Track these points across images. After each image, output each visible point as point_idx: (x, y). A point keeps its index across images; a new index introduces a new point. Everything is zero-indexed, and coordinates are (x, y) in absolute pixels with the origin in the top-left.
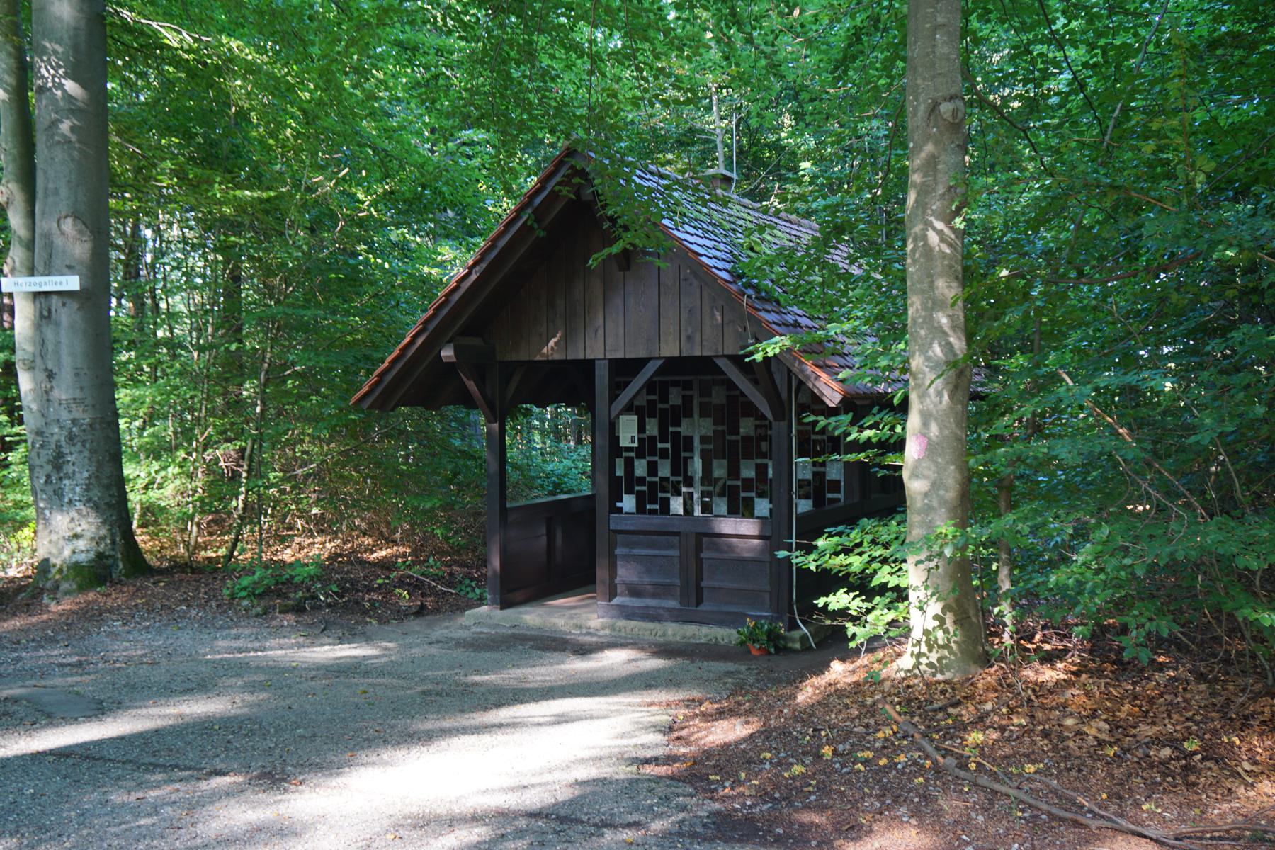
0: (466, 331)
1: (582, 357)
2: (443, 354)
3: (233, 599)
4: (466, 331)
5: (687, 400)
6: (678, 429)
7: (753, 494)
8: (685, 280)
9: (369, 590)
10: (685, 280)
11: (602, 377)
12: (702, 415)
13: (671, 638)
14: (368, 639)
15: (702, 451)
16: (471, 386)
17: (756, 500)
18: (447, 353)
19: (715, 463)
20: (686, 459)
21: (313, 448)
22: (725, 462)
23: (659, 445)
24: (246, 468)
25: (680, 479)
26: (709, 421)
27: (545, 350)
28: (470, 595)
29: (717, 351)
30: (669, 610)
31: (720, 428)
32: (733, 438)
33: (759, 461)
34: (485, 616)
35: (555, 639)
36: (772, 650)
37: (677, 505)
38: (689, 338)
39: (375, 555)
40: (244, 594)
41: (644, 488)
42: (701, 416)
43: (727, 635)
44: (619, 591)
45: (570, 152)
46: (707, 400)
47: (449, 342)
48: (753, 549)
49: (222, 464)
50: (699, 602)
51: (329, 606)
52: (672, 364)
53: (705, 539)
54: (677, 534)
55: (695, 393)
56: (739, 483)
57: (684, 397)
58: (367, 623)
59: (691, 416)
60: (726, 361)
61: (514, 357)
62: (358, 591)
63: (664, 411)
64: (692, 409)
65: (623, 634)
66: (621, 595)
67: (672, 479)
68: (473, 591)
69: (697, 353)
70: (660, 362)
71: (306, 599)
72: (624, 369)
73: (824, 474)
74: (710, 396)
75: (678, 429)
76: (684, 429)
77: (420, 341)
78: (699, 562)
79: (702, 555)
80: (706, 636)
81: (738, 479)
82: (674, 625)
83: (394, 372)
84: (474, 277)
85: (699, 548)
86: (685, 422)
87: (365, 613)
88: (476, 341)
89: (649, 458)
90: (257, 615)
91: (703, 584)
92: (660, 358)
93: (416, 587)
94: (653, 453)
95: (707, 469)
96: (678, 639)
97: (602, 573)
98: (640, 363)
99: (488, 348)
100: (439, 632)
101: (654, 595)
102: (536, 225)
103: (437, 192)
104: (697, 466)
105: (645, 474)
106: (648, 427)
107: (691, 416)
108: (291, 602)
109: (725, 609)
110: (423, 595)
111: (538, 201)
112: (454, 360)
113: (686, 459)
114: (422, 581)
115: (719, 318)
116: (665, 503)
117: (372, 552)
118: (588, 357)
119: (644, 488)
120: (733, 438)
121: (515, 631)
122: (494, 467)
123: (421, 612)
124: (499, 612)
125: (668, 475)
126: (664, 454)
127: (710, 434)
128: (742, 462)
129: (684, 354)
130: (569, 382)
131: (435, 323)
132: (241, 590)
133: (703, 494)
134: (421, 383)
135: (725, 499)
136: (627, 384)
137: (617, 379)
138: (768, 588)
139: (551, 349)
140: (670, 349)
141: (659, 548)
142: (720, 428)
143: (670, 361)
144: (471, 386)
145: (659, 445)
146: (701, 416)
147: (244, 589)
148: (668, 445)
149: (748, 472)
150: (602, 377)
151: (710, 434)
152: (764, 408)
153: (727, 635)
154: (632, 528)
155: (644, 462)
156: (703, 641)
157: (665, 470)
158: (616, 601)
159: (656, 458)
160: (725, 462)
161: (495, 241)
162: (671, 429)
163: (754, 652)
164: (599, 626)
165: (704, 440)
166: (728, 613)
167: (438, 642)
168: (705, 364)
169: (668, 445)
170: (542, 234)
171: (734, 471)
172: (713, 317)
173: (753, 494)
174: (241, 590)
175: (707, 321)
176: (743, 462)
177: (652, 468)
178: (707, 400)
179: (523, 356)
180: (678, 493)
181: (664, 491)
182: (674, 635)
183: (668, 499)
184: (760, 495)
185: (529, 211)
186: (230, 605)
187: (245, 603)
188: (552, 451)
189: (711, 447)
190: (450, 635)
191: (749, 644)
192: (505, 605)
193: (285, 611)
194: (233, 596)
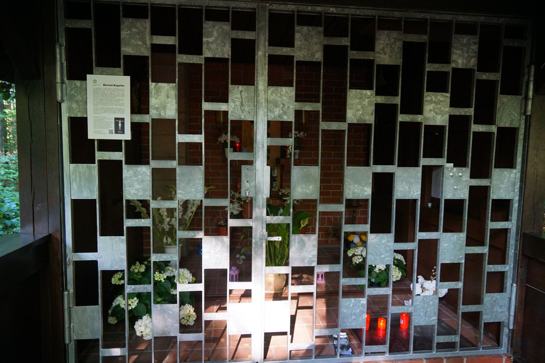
6: (222, 107)
12: (275, 81)
15: (269, 149)
19: (296, 172)
22: (315, 171)
23: (181, 138)
31: (308, 107)
32: (334, 126)
33: (380, 169)
46: (285, 51)
57: (235, 44)
59: (248, 80)
73: (485, 190)
74: (291, 44)
75: (222, 107)
76: (236, 105)
81: (338, 201)
86: (236, 93)
89: (154, 164)
104: (259, 178)
107: (248, 80)
113: (237, 167)
120: (334, 126)
126: (190, 155)
127: (290, 117)
133: (272, 229)
142: (308, 107)
145: (181, 138)
151: (290, 117)
157: (191, 185)
159: (173, 164)
160: (315, 171)
165: (277, 128)
169: (199, 138)
171: (331, 186)
173: (367, 227)
176: (350, 171)
178: (285, 51)
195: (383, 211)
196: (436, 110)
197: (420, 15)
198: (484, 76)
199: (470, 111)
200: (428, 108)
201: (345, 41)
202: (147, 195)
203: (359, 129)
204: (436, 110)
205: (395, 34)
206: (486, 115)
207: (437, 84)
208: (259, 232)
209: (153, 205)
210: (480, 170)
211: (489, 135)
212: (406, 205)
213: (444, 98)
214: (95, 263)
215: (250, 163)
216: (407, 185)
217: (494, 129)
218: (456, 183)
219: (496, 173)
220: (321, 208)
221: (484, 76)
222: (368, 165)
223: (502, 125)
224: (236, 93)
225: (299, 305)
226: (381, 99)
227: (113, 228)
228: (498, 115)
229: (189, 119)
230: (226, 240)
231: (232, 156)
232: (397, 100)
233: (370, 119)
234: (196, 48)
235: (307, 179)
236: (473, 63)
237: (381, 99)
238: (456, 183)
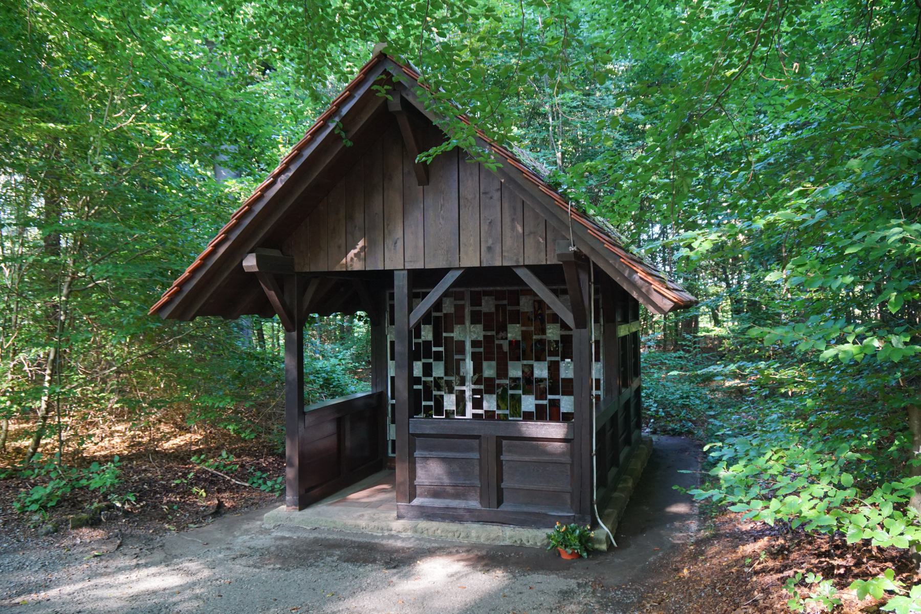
0: (267, 243)
1: (381, 268)
2: (244, 264)
3: (24, 512)
4: (267, 243)
5: (459, 309)
6: (452, 335)
8: (485, 193)
9: (167, 490)
10: (485, 193)
11: (401, 284)
12: (474, 321)
13: (474, 540)
14: (168, 560)
15: (473, 354)
16: (272, 295)
17: (523, 396)
18: (250, 262)
19: (485, 364)
20: (458, 361)
21: (118, 347)
22: (494, 363)
23: (434, 349)
24: (48, 372)
26: (479, 328)
27: (344, 260)
28: (263, 488)
29: (517, 261)
30: (470, 511)
31: (489, 333)
34: (283, 518)
35: (361, 546)
36: (585, 554)
37: (449, 402)
38: (489, 249)
39: (171, 442)
40: (35, 507)
41: (420, 387)
42: (472, 323)
43: (534, 537)
44: (418, 491)
45: (381, 58)
46: (478, 308)
47: (251, 252)
48: (559, 450)
49: (26, 368)
50: (500, 502)
51: (126, 513)
52: (472, 276)
53: (504, 442)
54: (478, 437)
55: (467, 303)
58: (166, 530)
60: (527, 271)
61: (313, 269)
62: (156, 492)
63: (437, 319)
64: (464, 317)
65: (425, 536)
66: (421, 496)
67: (445, 378)
68: (265, 483)
69: (498, 263)
70: (458, 273)
71: (102, 509)
72: (423, 279)
75: (452, 335)
76: (457, 334)
77: (222, 250)
78: (500, 464)
79: (502, 458)
80: (511, 538)
82: (476, 525)
83: (194, 282)
84: (279, 185)
85: (499, 452)
86: (457, 329)
87: (163, 518)
88: (276, 253)
89: (424, 361)
90: (47, 534)
91: (503, 485)
93: (212, 483)
94: (428, 356)
95: (478, 369)
96: (482, 540)
97: (401, 472)
99: (286, 258)
100: (241, 540)
101: (456, 496)
102: (343, 134)
103: (230, 121)
104: (469, 365)
105: (421, 375)
106: (423, 333)
108: (84, 515)
109: (526, 509)
110: (219, 491)
111: (345, 110)
112: (257, 270)
113: (458, 361)
114: (217, 476)
115: (520, 229)
116: (439, 402)
117: (168, 440)
119: (420, 387)
121: (315, 535)
122: (294, 373)
123: (219, 511)
124: (298, 513)
125: (442, 375)
126: (438, 357)
128: (510, 363)
129: (484, 265)
130: (367, 292)
131: (238, 232)
132: (33, 502)
133: (475, 392)
134: (222, 293)
136: (425, 295)
137: (414, 291)
138: (569, 488)
139: (353, 260)
140: (470, 260)
141: (459, 451)
142: (489, 333)
143: (469, 271)
144: (272, 295)
145: (434, 349)
146: (472, 323)
147: (36, 501)
148: (441, 349)
150: (401, 284)
152: (569, 319)
153: (534, 537)
154: (432, 432)
156: (508, 542)
157: (439, 370)
158: (416, 502)
159: (431, 361)
160: (494, 363)
161: (300, 150)
162: (444, 335)
163: (565, 557)
164: (401, 529)
165: (475, 344)
166: (534, 514)
167: (242, 556)
168: (505, 274)
169: (441, 349)
170: (349, 144)
171: (502, 371)
172: (513, 228)
173: (520, 392)
174: (33, 502)
175: (507, 232)
176: (510, 363)
177: (427, 370)
178: (478, 308)
179: (322, 266)
180: (451, 391)
181: (439, 389)
182: (478, 537)
183: (442, 396)
185: (337, 119)
186: (20, 520)
187: (35, 517)
188: (337, 353)
189: (482, 350)
190: (252, 544)
191: (561, 548)
192: (304, 503)
193: (78, 525)
194: (23, 509)
197: (477, 289)
200: (548, 331)
201: (505, 302)
202: (523, 396)
208: (468, 394)
209: (423, 379)
211: (419, 344)
215: (464, 360)
226: (524, 328)
229: (437, 341)
231: (456, 357)
235: (490, 367)
237: (524, 328)
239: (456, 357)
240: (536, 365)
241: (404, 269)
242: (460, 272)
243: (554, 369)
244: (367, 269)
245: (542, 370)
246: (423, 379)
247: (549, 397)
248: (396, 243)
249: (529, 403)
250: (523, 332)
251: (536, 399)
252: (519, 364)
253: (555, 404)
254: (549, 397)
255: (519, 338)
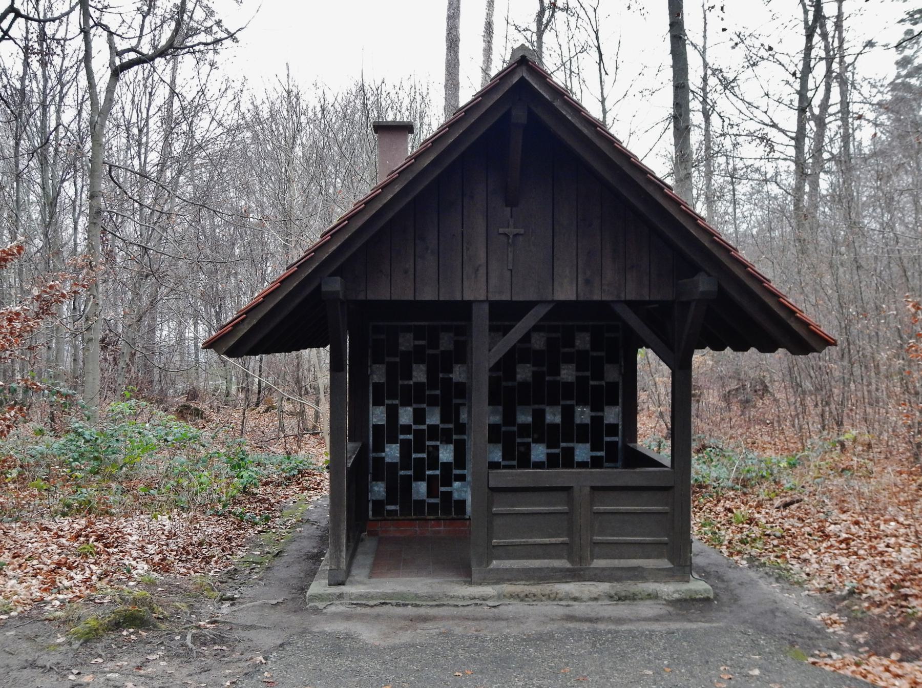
7: (530, 440)
17: (533, 445)
25: (451, 426)
30: (561, 570)
32: (510, 384)
33: (536, 407)
41: (410, 437)
56: (515, 429)
69: (596, 297)
70: (541, 311)
72: (504, 314)
73: (602, 418)
81: (514, 425)
89: (415, 406)
92: (553, 301)
94: (419, 400)
98: (525, 307)
106: (414, 373)
113: (458, 406)
118: (467, 297)
119: (410, 437)
120: (510, 384)
126: (433, 402)
128: (519, 408)
129: (581, 298)
135: (500, 446)
140: (566, 292)
149: (525, 418)
150: (481, 318)
155: (410, 409)
157: (434, 418)
159: (424, 406)
171: (510, 417)
176: (519, 408)
177: (419, 417)
180: (448, 441)
184: (536, 441)
195: (541, 431)
196: (568, 373)
198: (595, 354)
199: (588, 374)
200: (563, 372)
203: (524, 384)
204: (568, 373)
205: (542, 334)
206: (599, 375)
207: (568, 359)
209: (414, 427)
210: (597, 407)
212: (554, 426)
213: (572, 367)
214: (548, 447)
216: (553, 416)
217: (562, 402)
218: (583, 415)
219: (606, 409)
220: (503, 429)
221: (595, 354)
222: (529, 404)
223: (608, 380)
224: (457, 368)
225: (492, 484)
226: (535, 369)
227: (393, 440)
228: (606, 375)
229: (432, 380)
230: (452, 447)
231: (455, 401)
232: (545, 369)
233: (530, 379)
234: (437, 347)
236: (588, 346)
237: (535, 369)
238: (583, 415)
239: (455, 401)
240: (548, 409)
241: (487, 301)
242: (551, 306)
243: (568, 414)
244: (514, 299)
245: (555, 415)
246: (414, 427)
247: (563, 445)
248: (478, 270)
249: (539, 452)
250: (534, 373)
251: (592, 450)
252: (530, 409)
253: (570, 452)
254: (563, 445)
255: (530, 379)
